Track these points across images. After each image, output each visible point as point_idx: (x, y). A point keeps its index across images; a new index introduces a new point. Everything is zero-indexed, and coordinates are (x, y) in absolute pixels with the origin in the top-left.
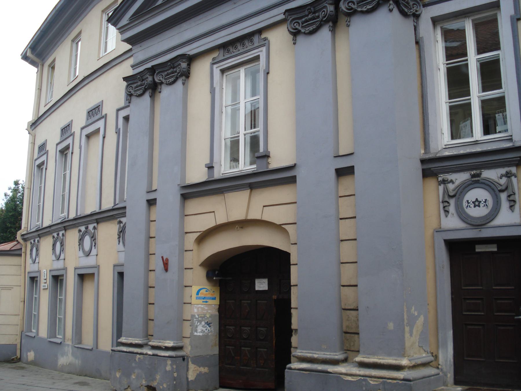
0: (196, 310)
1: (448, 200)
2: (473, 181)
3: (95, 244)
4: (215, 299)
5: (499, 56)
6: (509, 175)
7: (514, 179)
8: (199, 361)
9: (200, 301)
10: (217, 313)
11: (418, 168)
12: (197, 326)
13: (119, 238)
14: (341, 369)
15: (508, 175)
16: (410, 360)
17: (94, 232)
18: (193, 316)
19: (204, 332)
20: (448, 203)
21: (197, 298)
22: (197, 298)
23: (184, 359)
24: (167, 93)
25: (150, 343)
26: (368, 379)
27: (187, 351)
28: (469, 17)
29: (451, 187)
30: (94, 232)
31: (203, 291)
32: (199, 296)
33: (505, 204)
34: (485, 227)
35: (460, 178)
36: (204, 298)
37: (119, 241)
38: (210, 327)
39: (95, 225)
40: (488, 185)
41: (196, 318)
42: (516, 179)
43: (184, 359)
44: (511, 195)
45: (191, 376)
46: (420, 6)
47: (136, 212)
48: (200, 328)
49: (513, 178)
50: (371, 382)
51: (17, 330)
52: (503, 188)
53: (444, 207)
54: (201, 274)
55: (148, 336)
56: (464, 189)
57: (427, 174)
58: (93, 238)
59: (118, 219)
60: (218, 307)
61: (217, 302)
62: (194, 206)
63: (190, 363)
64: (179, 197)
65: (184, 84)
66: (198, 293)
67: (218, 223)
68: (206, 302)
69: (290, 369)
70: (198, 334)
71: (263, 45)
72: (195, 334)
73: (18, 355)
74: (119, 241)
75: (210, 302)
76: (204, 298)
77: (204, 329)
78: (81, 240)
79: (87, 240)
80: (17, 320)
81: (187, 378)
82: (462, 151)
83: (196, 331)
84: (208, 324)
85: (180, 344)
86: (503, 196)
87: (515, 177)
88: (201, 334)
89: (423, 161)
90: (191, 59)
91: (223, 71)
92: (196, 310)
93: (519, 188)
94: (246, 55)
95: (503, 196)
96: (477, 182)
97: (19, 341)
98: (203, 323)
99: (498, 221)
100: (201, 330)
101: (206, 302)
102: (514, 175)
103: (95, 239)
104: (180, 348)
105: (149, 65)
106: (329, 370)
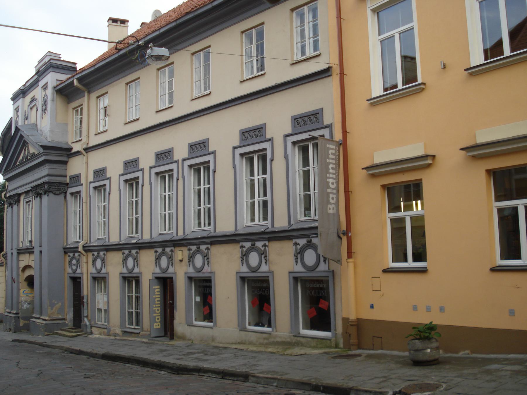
3: (172, 263)
7: (267, 248)
11: (63, 251)
13: (296, 259)
15: (265, 245)
17: (137, 256)
18: (22, 301)
24: (15, 207)
27: (20, 315)
30: (137, 256)
39: (105, 252)
45: (21, 324)
48: (25, 306)
55: (41, 314)
57: (65, 253)
58: (103, 261)
59: (188, 247)
62: (22, 257)
75: (30, 295)
78: (94, 261)
79: (99, 262)
89: (64, 248)
90: (19, 195)
99: (261, 270)
103: (172, 260)
104: (64, 319)
105: (34, 184)
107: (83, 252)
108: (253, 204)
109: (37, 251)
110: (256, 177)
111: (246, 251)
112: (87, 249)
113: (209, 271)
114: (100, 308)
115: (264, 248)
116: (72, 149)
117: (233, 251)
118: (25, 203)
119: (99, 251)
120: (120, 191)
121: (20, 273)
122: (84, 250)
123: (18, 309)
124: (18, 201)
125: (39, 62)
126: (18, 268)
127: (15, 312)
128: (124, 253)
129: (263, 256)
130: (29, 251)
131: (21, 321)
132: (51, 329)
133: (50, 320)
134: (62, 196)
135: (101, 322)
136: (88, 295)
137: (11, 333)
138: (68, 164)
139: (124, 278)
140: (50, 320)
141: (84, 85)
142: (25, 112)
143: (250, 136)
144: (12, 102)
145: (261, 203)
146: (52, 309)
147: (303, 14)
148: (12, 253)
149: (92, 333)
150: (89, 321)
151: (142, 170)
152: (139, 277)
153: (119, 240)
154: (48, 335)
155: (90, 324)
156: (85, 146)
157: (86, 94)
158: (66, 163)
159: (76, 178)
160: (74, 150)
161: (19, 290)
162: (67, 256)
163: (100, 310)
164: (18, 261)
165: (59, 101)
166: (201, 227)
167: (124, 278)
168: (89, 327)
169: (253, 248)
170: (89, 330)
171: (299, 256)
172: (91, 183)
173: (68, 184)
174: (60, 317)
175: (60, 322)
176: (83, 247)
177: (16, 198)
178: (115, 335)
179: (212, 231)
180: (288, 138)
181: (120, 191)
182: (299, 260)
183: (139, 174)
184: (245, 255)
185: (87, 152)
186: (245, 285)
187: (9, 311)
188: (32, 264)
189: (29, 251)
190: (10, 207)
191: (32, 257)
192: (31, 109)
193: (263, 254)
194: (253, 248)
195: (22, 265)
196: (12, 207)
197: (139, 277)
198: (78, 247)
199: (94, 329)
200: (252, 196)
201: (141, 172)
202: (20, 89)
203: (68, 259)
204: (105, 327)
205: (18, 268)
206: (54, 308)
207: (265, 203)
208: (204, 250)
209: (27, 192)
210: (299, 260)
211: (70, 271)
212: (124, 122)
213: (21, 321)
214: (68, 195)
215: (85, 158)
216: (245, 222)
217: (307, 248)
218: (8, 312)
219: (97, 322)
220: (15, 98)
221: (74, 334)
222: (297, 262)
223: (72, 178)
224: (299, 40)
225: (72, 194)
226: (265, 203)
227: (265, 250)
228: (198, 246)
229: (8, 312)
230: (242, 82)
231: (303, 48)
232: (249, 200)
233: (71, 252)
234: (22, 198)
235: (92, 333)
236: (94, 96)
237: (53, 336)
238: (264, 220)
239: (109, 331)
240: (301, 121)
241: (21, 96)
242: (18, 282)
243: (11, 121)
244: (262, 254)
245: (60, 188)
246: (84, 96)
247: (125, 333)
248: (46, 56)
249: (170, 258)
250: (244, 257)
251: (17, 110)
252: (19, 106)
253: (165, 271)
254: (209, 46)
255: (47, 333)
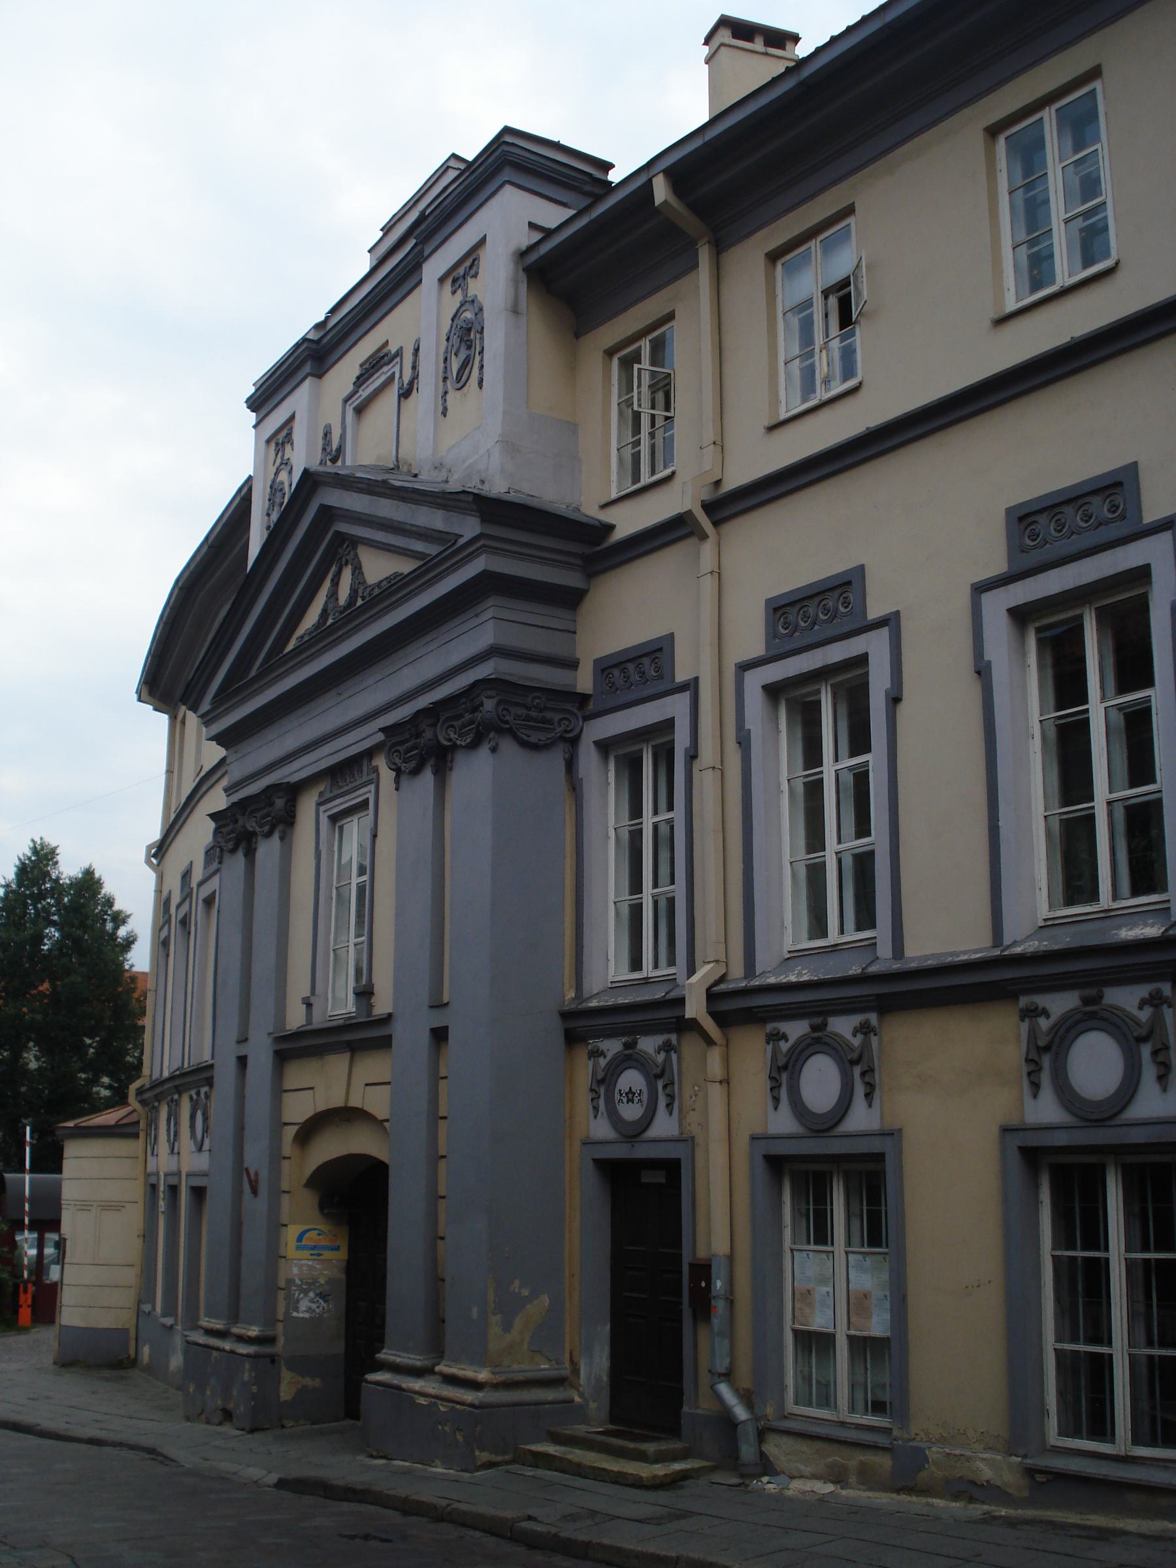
0: (295, 1270)
1: (1036, 1058)
2: (1086, 1013)
4: (337, 1249)
5: (1150, 701)
6: (1156, 1002)
8: (300, 1365)
9: (306, 1254)
10: (343, 1276)
11: (556, 1028)
12: (298, 1301)
13: (775, 1088)
14: (417, 1384)
16: (493, 1373)
18: (290, 1281)
19: (314, 1311)
20: (1037, 1063)
21: (298, 1248)
22: (298, 1248)
23: (273, 1361)
24: (268, 850)
25: (235, 1330)
26: (439, 1402)
28: (1090, 603)
29: (1044, 1024)
31: (313, 1234)
32: (304, 1243)
33: (1149, 1072)
34: (1112, 1123)
35: (1060, 1004)
36: (314, 1248)
37: (596, 1109)
38: (325, 1301)
40: (834, 1048)
41: (297, 1286)
42: (1171, 1010)
43: (273, 1361)
44: (1160, 1049)
45: (286, 1393)
46: (577, 718)
47: (225, 1076)
48: (304, 1304)
49: (1165, 1008)
50: (442, 1408)
51: (127, 1299)
52: (1144, 1032)
53: (1029, 1074)
54: (308, 1201)
56: (1067, 1031)
57: (572, 1039)
60: (344, 1264)
61: (343, 1254)
62: (298, 1074)
63: (283, 1368)
64: (271, 1054)
65: (282, 838)
66: (300, 1239)
67: (319, 1109)
68: (319, 1255)
69: (367, 1381)
70: (301, 1315)
71: (369, 782)
72: (295, 1314)
73: (132, 1352)
74: (776, 1100)
75: (327, 1254)
76: (314, 1248)
77: (314, 1306)
80: (131, 1276)
81: (279, 1397)
82: (622, 1000)
83: (297, 1309)
84: (323, 1296)
85: (269, 1333)
86: (1146, 1050)
87: (1170, 1007)
88: (307, 1315)
89: (565, 1015)
90: (293, 791)
91: (334, 819)
92: (295, 1270)
93: (680, 1073)
94: (354, 795)
95: (1146, 1050)
96: (1092, 1016)
97: (134, 1322)
98: (311, 1294)
99: (655, 1131)
100: (306, 1307)
101: (319, 1255)
102: (1165, 1002)
106: (404, 1385)
107: (709, 1025)
108: (636, 911)
109: (410, 1036)
110: (828, 770)
111: (1056, 1028)
112: (736, 1008)
113: (875, 1125)
114: (819, 1322)
115: (860, 1037)
116: (610, 528)
117: (988, 1039)
118: (324, 819)
119: (819, 1012)
120: (982, 671)
121: (288, 1147)
122: (713, 1014)
123: (271, 1321)
124: (288, 820)
125: (387, 230)
126: (278, 1124)
127: (254, 1331)
128: (775, 1037)
129: (857, 1071)
130: (363, 1035)
131: (287, 1376)
132: (500, 1432)
133: (496, 1386)
134: (555, 760)
135: (826, 1400)
136: (731, 1258)
137: (227, 1429)
138: (588, 604)
139: (776, 1164)
140: (496, 1386)
141: (699, 209)
142: (327, 434)
143: (826, 611)
144: (252, 417)
145: (848, 861)
146: (507, 1327)
147: (1040, 144)
148: (242, 1061)
149: (766, 1467)
150: (747, 1398)
151: (692, 686)
152: (880, 1157)
153: (988, 942)
154: (491, 1465)
155: (757, 1419)
156: (706, 495)
157: (704, 255)
158: (571, 599)
159: (645, 667)
160: (619, 534)
161: (276, 1227)
162: (581, 1054)
163: (814, 1344)
164: (278, 1091)
165: (538, 331)
166: (824, 934)
167: (776, 1164)
168: (752, 1434)
169: (818, 1041)
170: (747, 1452)
171: (1046, 1061)
172: (745, 667)
173: (584, 698)
174: (544, 1367)
175: (550, 1395)
176: (712, 996)
177: (280, 803)
178: (969, 1489)
179: (885, 950)
180: (987, 599)
181: (982, 671)
182: (784, 1093)
183: (676, 707)
184: (785, 1067)
185: (716, 524)
186: (1036, 1186)
187: (218, 1325)
188: (378, 1103)
189: (363, 1035)
190: (240, 856)
191: (374, 1067)
192: (360, 411)
193: (857, 1062)
194: (629, 1059)
195: (299, 1109)
196: (250, 854)
197: (880, 1157)
198: (681, 1002)
199: (775, 1448)
200: (815, 840)
201: (684, 698)
202: (304, 340)
203: (584, 1070)
204: (881, 1440)
205: (278, 1124)
206: (518, 1323)
207: (864, 863)
208: (1135, 1012)
209: (342, 772)
210: (784, 1093)
211: (601, 1129)
212: (767, 422)
213: (287, 1376)
214: (588, 757)
215: (707, 550)
216: (1034, 905)
217: (811, 1050)
218: (210, 1332)
219: (791, 1407)
220: (263, 399)
221: (660, 1470)
222: (776, 1100)
223: (606, 667)
224: (796, 351)
225: (604, 747)
226: (864, 863)
227: (866, 1045)
228: (817, 1020)
229: (210, 1332)
230: (772, 428)
231: (809, 375)
232: (802, 854)
233: (611, 1033)
234: (307, 808)
235: (766, 1467)
236: (748, 259)
237: (514, 1467)
238: (859, 928)
239: (918, 1458)
240: (802, 614)
241: (307, 368)
242: (277, 1192)
243: (250, 490)
244: (853, 1063)
245: (549, 715)
246: (696, 266)
247: (1050, 1483)
248: (444, 168)
249: (660, 1076)
250: (784, 1077)
251: (280, 440)
252: (292, 418)
253: (634, 1132)
254: (670, 317)
255: (483, 1456)
